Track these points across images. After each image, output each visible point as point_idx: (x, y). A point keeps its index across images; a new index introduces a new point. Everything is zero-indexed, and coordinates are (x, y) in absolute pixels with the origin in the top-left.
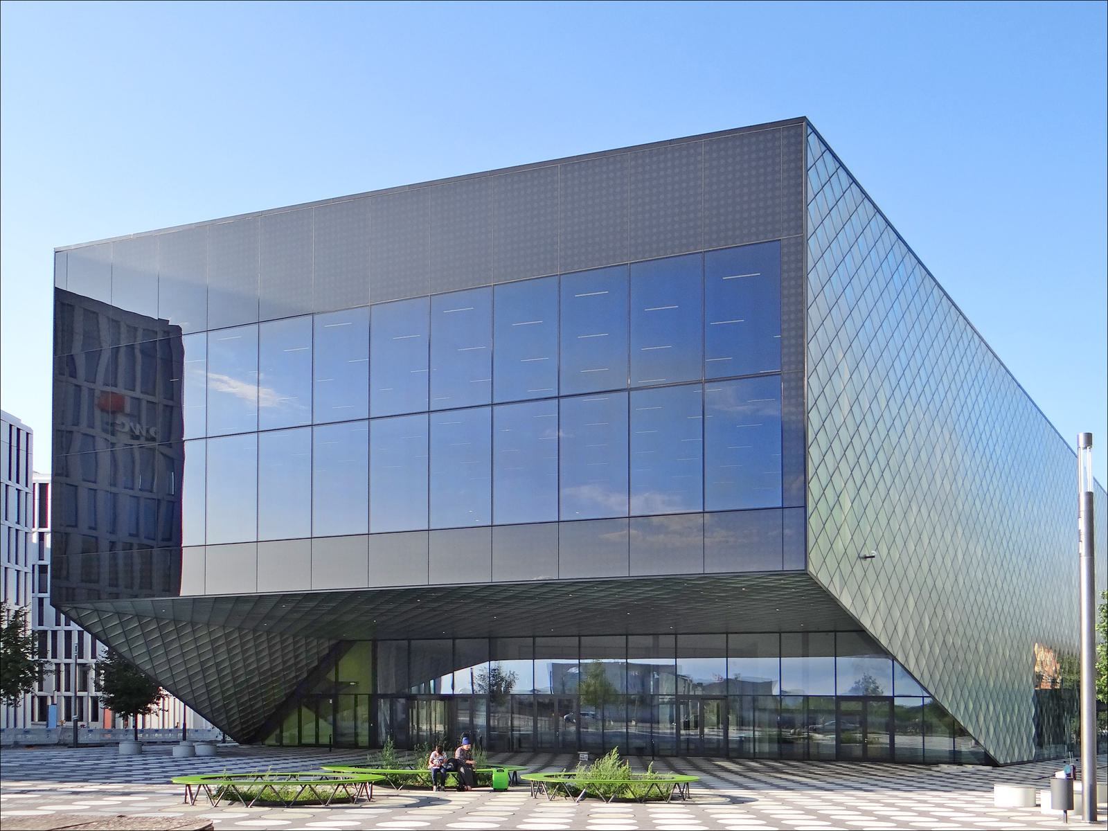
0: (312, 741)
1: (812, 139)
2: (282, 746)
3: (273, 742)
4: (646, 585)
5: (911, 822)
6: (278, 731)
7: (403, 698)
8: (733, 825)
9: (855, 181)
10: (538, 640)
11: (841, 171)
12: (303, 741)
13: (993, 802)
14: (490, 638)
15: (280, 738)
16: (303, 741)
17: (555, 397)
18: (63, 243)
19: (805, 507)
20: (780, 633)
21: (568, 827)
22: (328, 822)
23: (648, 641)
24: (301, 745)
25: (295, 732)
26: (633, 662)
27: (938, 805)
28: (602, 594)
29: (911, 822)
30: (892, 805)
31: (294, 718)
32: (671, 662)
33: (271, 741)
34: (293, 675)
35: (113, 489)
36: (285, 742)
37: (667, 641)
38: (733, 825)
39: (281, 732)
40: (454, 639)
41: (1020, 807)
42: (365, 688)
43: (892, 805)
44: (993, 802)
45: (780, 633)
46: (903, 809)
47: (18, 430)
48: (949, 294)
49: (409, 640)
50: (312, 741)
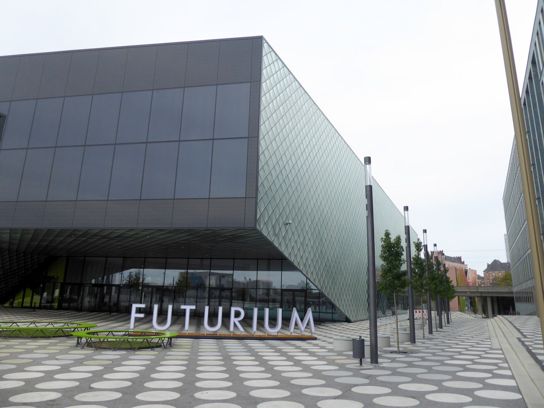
0: (29, 305)
1: (265, 45)
2: (12, 307)
4: (181, 233)
5: (345, 359)
6: (12, 300)
7: (148, 286)
10: (108, 259)
12: (24, 305)
14: (124, 257)
15: (12, 303)
16: (24, 305)
17: (118, 144)
18: (265, 36)
20: (258, 259)
21: (168, 353)
22: (446, 367)
23: (198, 261)
24: (22, 307)
25: (21, 300)
28: (163, 236)
29: (345, 359)
32: (230, 272)
33: (7, 305)
34: (23, 272)
37: (207, 262)
39: (14, 300)
40: (107, 257)
41: (345, 351)
42: (61, 280)
45: (258, 259)
50: (29, 305)
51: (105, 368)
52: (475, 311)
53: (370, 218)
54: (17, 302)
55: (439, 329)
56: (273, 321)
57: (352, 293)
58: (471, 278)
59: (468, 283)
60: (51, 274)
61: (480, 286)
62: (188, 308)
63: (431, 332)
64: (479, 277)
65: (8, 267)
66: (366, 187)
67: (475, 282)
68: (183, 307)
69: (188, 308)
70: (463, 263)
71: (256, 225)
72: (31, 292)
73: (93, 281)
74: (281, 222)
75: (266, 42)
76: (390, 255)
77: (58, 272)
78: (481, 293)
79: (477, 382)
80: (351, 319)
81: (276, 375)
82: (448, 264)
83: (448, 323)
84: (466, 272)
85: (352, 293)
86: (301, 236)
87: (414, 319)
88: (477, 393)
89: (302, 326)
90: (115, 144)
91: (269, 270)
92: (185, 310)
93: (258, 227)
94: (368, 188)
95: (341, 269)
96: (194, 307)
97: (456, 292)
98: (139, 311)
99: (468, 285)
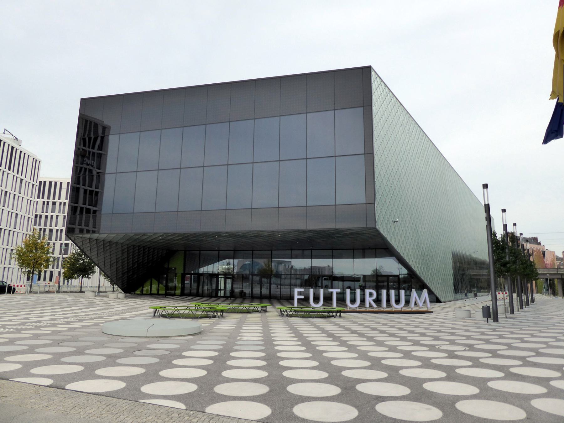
0: (156, 292)
1: (373, 73)
3: (140, 293)
6: (141, 288)
8: (300, 351)
9: (387, 86)
11: (382, 83)
13: (64, 186)
15: (142, 291)
18: (372, 66)
19: (373, 153)
23: (300, 252)
26: (475, 375)
27: (407, 325)
30: (379, 323)
31: (148, 283)
33: (138, 292)
35: (78, 186)
36: (144, 292)
37: (307, 253)
38: (300, 351)
39: (143, 288)
42: (180, 270)
43: (379, 323)
44: (64, 186)
46: (384, 324)
47: (21, 152)
48: (243, 378)
49: (200, 251)
50: (156, 292)
51: (85, 368)
52: (554, 294)
53: (489, 227)
54: (146, 288)
55: (509, 315)
56: (398, 301)
57: (440, 276)
58: (549, 259)
59: (546, 264)
60: (172, 265)
61: (559, 268)
62: (335, 291)
63: (522, 308)
64: (558, 259)
65: (141, 260)
66: (485, 205)
67: (553, 264)
68: (331, 290)
69: (335, 291)
70: (540, 244)
71: (375, 225)
72: (157, 282)
73: (192, 272)
74: (391, 221)
75: (374, 70)
76: (498, 249)
77: (177, 264)
78: (561, 275)
79: (554, 369)
80: (442, 300)
81: (325, 364)
82: (528, 246)
83: (533, 302)
84: (544, 253)
85: (440, 276)
86: (404, 230)
87: (496, 300)
88: (553, 383)
89: (420, 303)
90: (253, 163)
91: (364, 257)
92: (332, 293)
93: (377, 227)
94: (487, 206)
95: (432, 256)
96: (339, 290)
97: (539, 274)
98: (300, 293)
99: (546, 267)
